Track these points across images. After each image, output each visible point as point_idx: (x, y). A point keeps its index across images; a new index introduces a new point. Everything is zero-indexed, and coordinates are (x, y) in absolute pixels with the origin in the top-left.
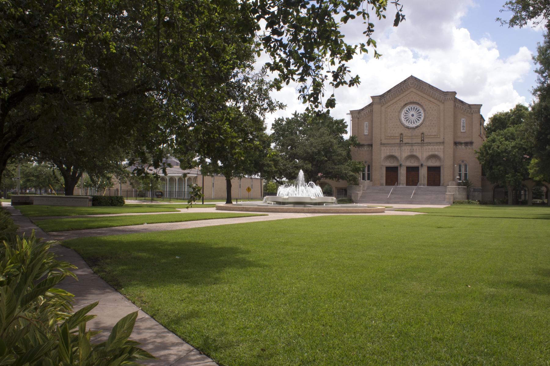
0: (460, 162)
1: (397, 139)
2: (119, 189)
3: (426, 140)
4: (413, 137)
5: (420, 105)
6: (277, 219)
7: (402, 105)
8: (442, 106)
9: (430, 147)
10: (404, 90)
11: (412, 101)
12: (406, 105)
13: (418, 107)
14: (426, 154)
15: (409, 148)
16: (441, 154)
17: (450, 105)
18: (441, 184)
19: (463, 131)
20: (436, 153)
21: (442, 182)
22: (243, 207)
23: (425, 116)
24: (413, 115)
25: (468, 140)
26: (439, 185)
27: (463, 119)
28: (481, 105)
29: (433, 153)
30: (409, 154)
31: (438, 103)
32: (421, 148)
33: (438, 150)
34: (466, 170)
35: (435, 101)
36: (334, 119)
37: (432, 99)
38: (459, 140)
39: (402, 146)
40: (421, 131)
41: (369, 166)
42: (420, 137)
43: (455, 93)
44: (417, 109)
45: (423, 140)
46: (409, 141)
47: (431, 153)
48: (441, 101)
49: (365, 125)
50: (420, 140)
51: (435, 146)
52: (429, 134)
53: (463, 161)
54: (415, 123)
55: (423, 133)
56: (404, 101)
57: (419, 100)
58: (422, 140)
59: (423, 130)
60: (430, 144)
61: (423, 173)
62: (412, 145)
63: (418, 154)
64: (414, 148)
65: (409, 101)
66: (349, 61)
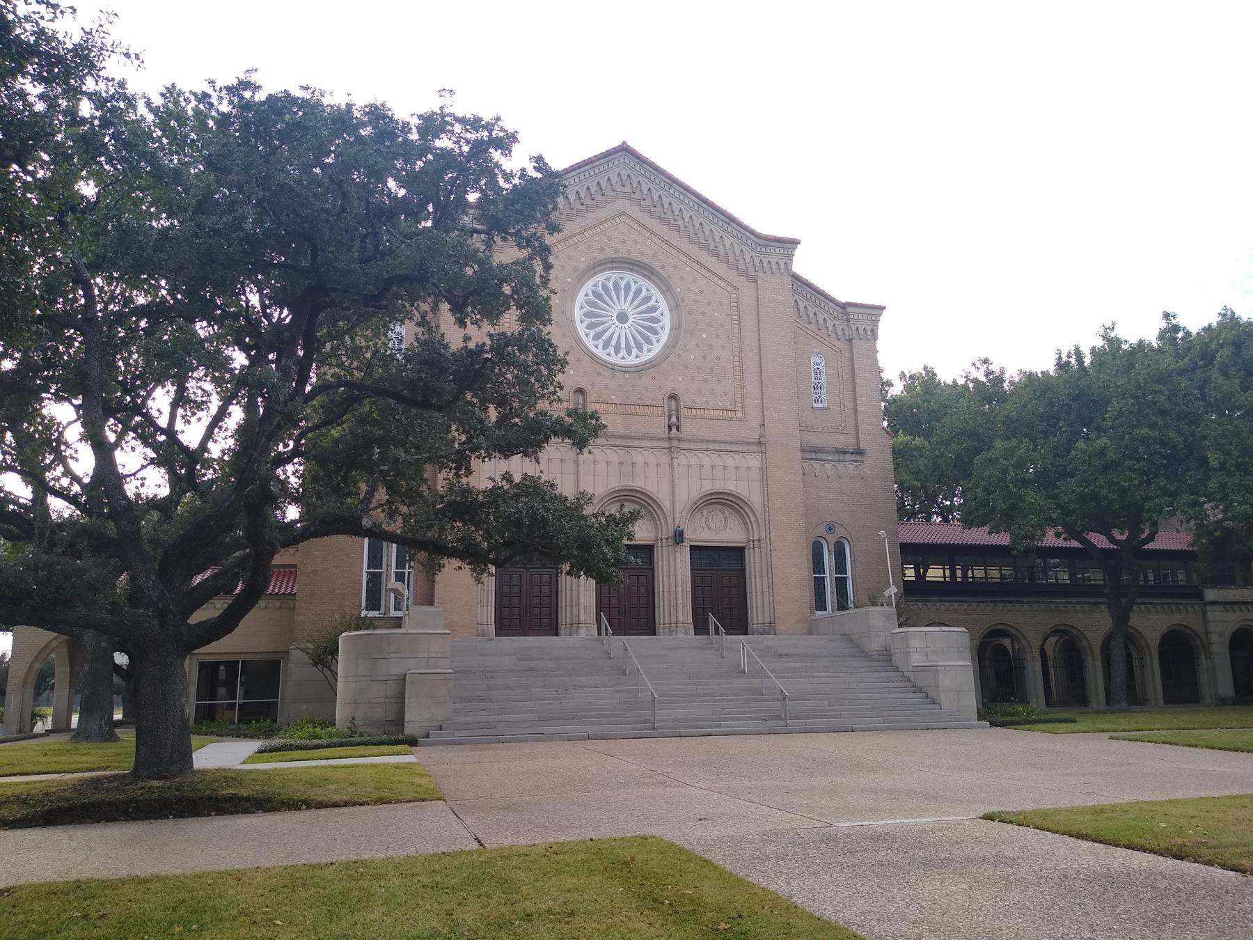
0: (822, 531)
1: (209, 435)
2: (402, 631)
5: (658, 276)
7: (582, 266)
10: (588, 201)
11: (622, 253)
12: (616, 263)
13: (644, 283)
14: (690, 487)
16: (751, 492)
20: (731, 487)
23: (676, 329)
24: (622, 317)
26: (651, 630)
28: (885, 308)
29: (719, 486)
31: (732, 276)
32: (665, 459)
34: (840, 566)
35: (721, 268)
37: (705, 258)
40: (668, 389)
41: (821, 605)
43: (789, 245)
44: (638, 291)
47: (708, 487)
48: (745, 273)
50: (664, 422)
52: (700, 405)
53: (830, 529)
55: (673, 397)
56: (589, 248)
57: (656, 255)
58: (670, 428)
59: (677, 383)
60: (706, 445)
64: (638, 457)
65: (609, 254)
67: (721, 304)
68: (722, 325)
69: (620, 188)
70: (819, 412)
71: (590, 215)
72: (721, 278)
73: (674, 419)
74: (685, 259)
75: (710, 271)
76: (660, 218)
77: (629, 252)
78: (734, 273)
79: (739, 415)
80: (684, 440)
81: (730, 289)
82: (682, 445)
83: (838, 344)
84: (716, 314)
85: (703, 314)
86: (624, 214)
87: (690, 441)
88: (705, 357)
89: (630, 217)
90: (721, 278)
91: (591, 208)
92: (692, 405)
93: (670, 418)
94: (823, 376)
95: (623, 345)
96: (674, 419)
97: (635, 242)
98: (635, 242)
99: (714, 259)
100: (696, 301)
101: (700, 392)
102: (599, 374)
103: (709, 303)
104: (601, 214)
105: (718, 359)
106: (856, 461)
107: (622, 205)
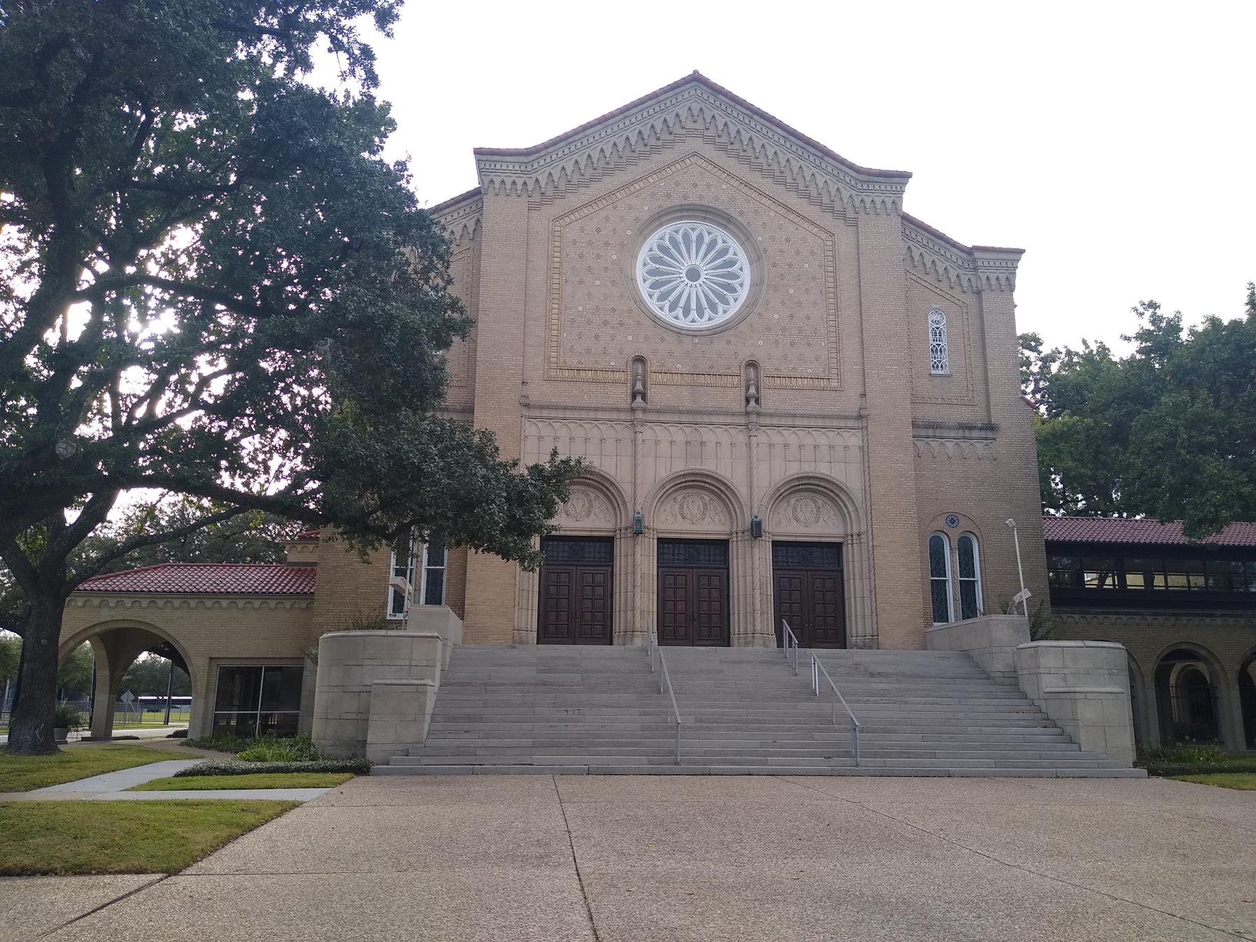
3: (771, 401)
4: (702, 379)
9: (792, 438)
11: (693, 199)
15: (679, 435)
16: (848, 476)
18: (734, 639)
20: (823, 469)
30: (680, 467)
31: (827, 220)
35: (813, 212)
37: (793, 200)
45: (757, 401)
46: (680, 396)
47: (794, 470)
48: (843, 215)
49: (931, 326)
51: (846, 435)
52: (786, 373)
53: (953, 521)
56: (653, 195)
57: (733, 199)
58: (634, 396)
59: (759, 348)
60: (791, 420)
62: (695, 417)
64: (708, 435)
67: (813, 253)
68: (814, 278)
69: (690, 125)
70: (938, 380)
71: (655, 157)
72: (813, 223)
75: (799, 215)
76: (738, 156)
77: (701, 197)
78: (829, 216)
79: (834, 384)
80: (765, 415)
82: (763, 421)
83: (962, 297)
84: (806, 266)
85: (790, 265)
86: (695, 154)
87: (772, 415)
88: (791, 316)
89: (703, 157)
90: (813, 223)
91: (656, 149)
92: (775, 373)
93: (748, 389)
96: (752, 390)
98: (709, 186)
99: (804, 201)
100: (782, 251)
101: (785, 357)
102: (663, 339)
103: (798, 253)
104: (668, 155)
105: (808, 318)
106: (986, 439)
107: (695, 144)
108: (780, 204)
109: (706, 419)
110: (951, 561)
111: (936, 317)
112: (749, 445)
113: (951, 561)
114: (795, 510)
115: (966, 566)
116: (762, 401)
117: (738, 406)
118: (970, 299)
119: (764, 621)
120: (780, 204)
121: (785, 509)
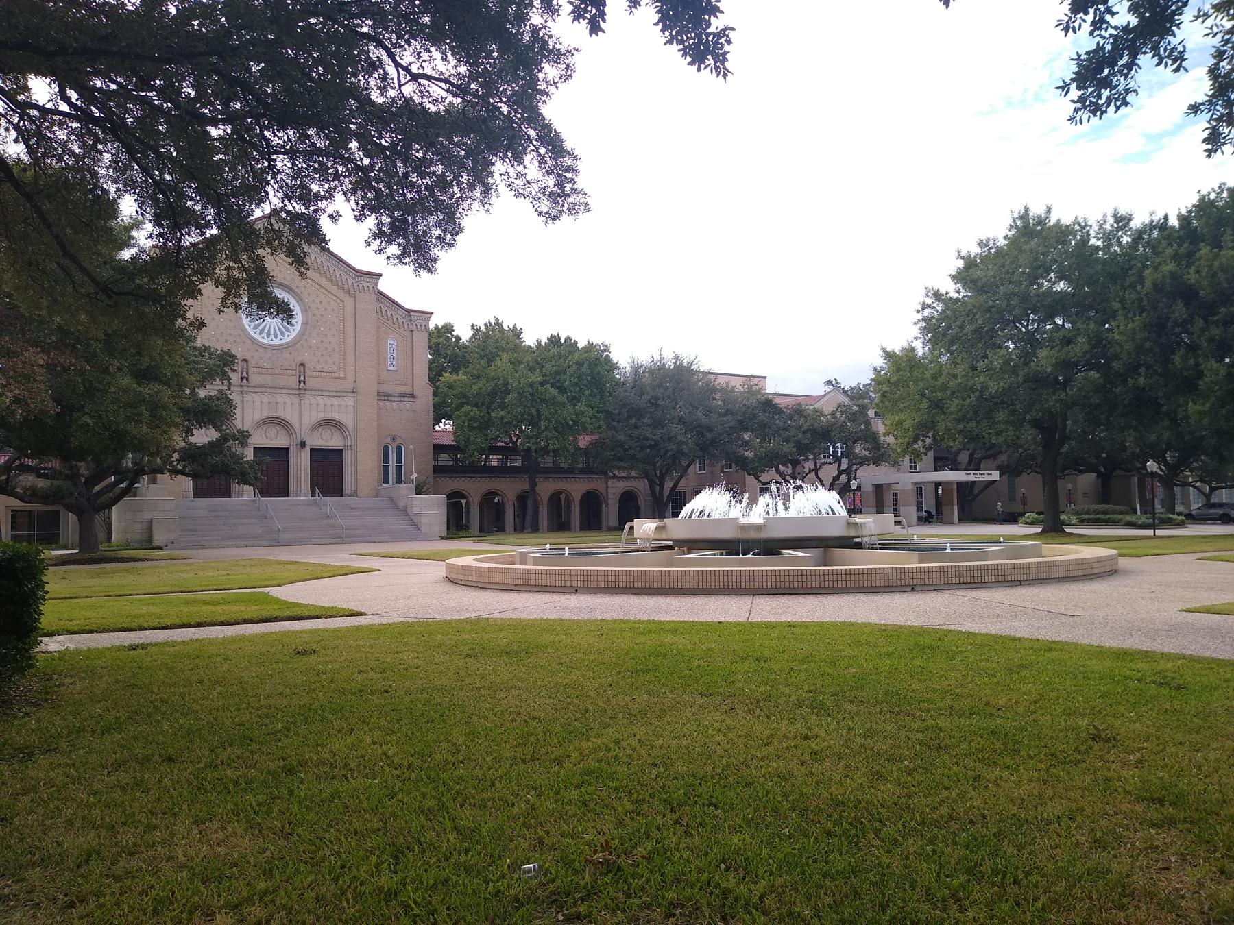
0: (389, 440)
3: (311, 383)
5: (294, 292)
6: (1047, 635)
8: (349, 303)
9: (321, 401)
15: (265, 398)
16: (347, 420)
17: (367, 304)
18: (291, 493)
19: (392, 368)
20: (335, 416)
21: (348, 486)
22: (984, 568)
25: (403, 390)
26: (340, 493)
27: (392, 342)
29: (328, 416)
30: (265, 414)
31: (340, 293)
33: (340, 410)
34: (399, 459)
35: (333, 288)
36: (529, 339)
38: (386, 388)
39: (247, 392)
40: (299, 359)
42: (308, 373)
45: (247, 379)
46: (268, 380)
47: (322, 416)
49: (389, 346)
51: (347, 400)
52: (319, 369)
54: (272, 337)
58: (242, 379)
59: (306, 357)
61: (300, 466)
62: (273, 390)
63: (293, 418)
64: (280, 399)
66: (999, 231)
68: (333, 323)
73: (302, 378)
74: (311, 282)
79: (342, 375)
81: (339, 301)
82: (307, 392)
85: (322, 316)
93: (242, 373)
94: (395, 351)
95: (266, 331)
96: (302, 378)
97: (280, 271)
99: (330, 283)
101: (318, 361)
102: (257, 351)
103: (326, 309)
108: (317, 284)
109: (279, 391)
110: (392, 456)
111: (392, 342)
112: (300, 404)
113: (392, 456)
114: (266, 432)
115: (399, 459)
116: (307, 383)
117: (295, 385)
118: (407, 333)
119: (306, 485)
120: (317, 284)
121: (316, 434)
